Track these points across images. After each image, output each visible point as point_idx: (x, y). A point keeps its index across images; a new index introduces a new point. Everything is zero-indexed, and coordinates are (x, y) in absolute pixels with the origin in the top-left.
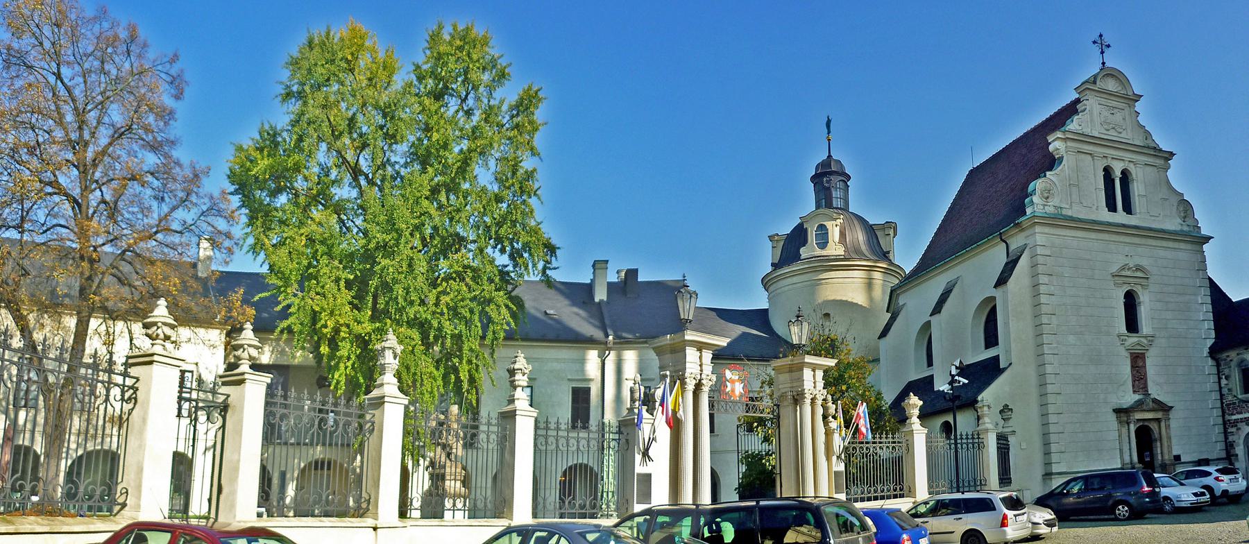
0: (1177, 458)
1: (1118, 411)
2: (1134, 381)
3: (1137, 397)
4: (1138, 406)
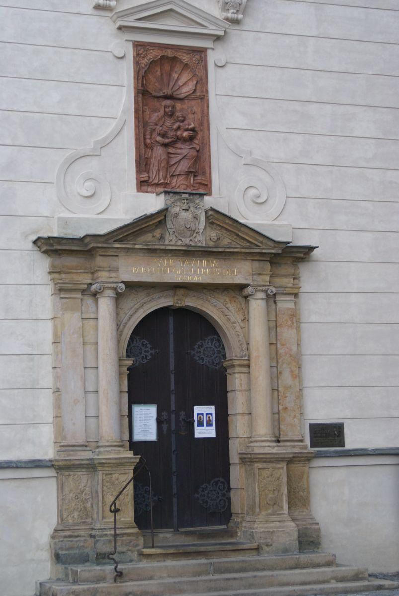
0: (328, 436)
1: (52, 247)
2: (143, 146)
3: (153, 203)
4: (137, 234)
